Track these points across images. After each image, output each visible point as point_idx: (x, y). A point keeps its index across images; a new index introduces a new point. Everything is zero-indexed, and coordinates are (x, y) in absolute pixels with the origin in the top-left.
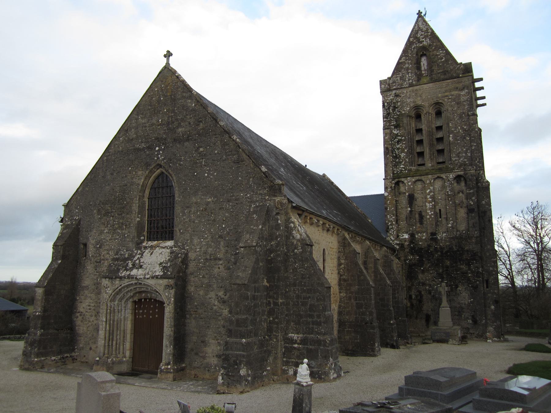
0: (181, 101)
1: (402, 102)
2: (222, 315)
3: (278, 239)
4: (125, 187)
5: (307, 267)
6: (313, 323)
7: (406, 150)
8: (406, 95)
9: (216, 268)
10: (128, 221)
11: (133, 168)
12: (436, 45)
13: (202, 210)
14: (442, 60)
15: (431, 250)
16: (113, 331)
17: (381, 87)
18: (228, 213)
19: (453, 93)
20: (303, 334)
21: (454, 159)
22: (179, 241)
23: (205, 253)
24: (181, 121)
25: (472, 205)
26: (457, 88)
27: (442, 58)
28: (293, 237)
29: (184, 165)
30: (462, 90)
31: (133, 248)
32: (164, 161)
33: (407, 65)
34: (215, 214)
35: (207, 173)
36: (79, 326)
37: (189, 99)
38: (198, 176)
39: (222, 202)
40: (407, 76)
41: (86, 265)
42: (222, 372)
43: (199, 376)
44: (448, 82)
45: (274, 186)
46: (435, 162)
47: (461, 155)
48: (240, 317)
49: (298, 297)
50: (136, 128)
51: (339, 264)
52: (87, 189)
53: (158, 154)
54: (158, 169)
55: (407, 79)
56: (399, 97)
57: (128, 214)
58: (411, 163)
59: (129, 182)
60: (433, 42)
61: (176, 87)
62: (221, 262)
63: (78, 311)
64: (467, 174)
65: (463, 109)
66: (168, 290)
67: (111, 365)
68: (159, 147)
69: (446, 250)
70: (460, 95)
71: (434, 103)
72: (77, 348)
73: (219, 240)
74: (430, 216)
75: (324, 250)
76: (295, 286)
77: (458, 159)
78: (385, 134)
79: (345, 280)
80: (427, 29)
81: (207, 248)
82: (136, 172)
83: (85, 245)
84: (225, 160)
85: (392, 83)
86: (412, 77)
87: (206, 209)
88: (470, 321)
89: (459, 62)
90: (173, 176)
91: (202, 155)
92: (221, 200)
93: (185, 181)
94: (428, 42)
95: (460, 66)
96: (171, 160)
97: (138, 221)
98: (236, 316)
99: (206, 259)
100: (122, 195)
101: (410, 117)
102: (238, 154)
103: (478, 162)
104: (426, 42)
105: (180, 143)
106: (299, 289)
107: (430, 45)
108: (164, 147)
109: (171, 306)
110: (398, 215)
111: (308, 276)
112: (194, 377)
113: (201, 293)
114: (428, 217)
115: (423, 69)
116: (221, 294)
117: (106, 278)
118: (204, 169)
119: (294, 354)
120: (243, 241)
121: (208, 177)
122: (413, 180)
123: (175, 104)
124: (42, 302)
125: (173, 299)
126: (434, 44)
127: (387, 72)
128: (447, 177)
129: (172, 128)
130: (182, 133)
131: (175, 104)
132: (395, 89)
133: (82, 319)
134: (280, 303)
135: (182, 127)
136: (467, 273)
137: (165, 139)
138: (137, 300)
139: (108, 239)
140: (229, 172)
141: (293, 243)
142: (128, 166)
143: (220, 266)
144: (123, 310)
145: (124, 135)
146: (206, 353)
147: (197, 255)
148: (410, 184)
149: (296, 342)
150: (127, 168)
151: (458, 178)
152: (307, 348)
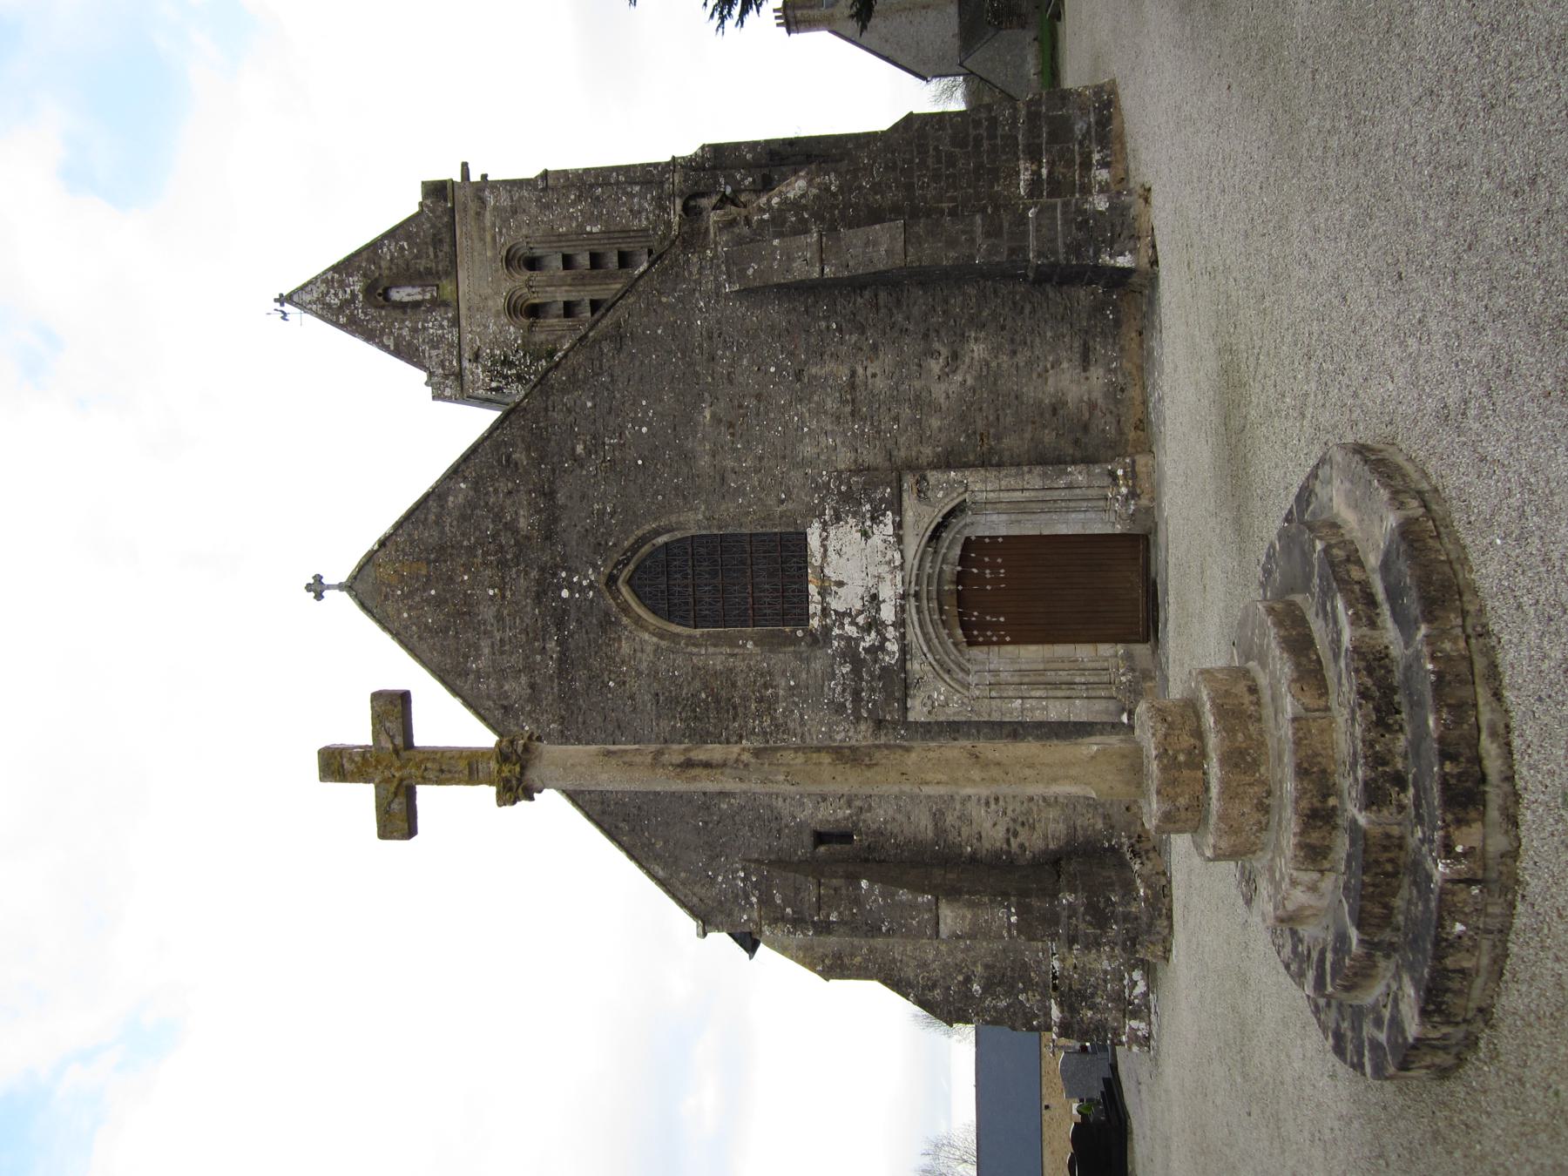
0: (447, 529)
1: (495, 343)
2: (985, 360)
3: (806, 216)
4: (661, 698)
5: (869, 157)
6: (992, 137)
8: (479, 334)
9: (873, 386)
10: (755, 682)
11: (610, 671)
13: (733, 435)
14: (406, 247)
18: (741, 358)
19: (488, 224)
20: (1018, 159)
21: (645, 223)
22: (809, 503)
23: (838, 418)
24: (501, 522)
25: (754, 180)
26: (478, 214)
27: (402, 248)
28: (803, 196)
29: (615, 501)
30: (483, 203)
31: (827, 654)
32: (601, 566)
33: (405, 332)
34: (744, 396)
35: (641, 427)
37: (447, 502)
38: (647, 453)
39: (713, 379)
40: (431, 331)
41: (874, 827)
42: (1108, 258)
43: (1138, 416)
44: (461, 235)
45: (683, 237)
48: (979, 230)
49: (936, 177)
50: (502, 674)
52: (659, 845)
53: (582, 590)
54: (618, 590)
56: (480, 352)
57: (734, 685)
59: (649, 686)
61: (407, 549)
62: (860, 371)
63: (1005, 846)
64: (681, 190)
66: (929, 494)
67: (1137, 674)
68: (561, 589)
70: (495, 208)
71: (507, 268)
72: (1109, 841)
73: (806, 380)
76: (912, 185)
77: (644, 214)
80: (326, 281)
81: (825, 413)
82: (623, 662)
84: (612, 376)
85: (443, 369)
86: (436, 320)
87: (731, 425)
89: (415, 209)
90: (639, 533)
91: (595, 446)
92: (710, 379)
93: (657, 493)
94: (356, 279)
95: (427, 206)
96: (600, 544)
97: (755, 644)
98: (979, 241)
99: (853, 414)
100: (683, 708)
101: (532, 325)
102: (600, 342)
104: (356, 284)
105: (556, 520)
106: (919, 177)
107: (365, 275)
108: (564, 569)
109: (970, 479)
111: (889, 155)
112: (1143, 430)
113: (935, 423)
115: (419, 297)
116: (935, 366)
117: (906, 709)
118: (629, 436)
119: (1063, 174)
120: (808, 271)
121: (649, 425)
123: (453, 547)
124: (979, 905)
125: (953, 473)
129: (515, 549)
130: (532, 515)
131: (453, 547)
132: (460, 361)
133: (1027, 827)
134: (951, 205)
135: (515, 520)
137: (542, 570)
140: (642, 362)
141: (817, 197)
142: (605, 690)
143: (869, 373)
145: (518, 719)
146: (1081, 400)
147: (843, 443)
149: (1037, 173)
150: (610, 696)
152: (1047, 143)
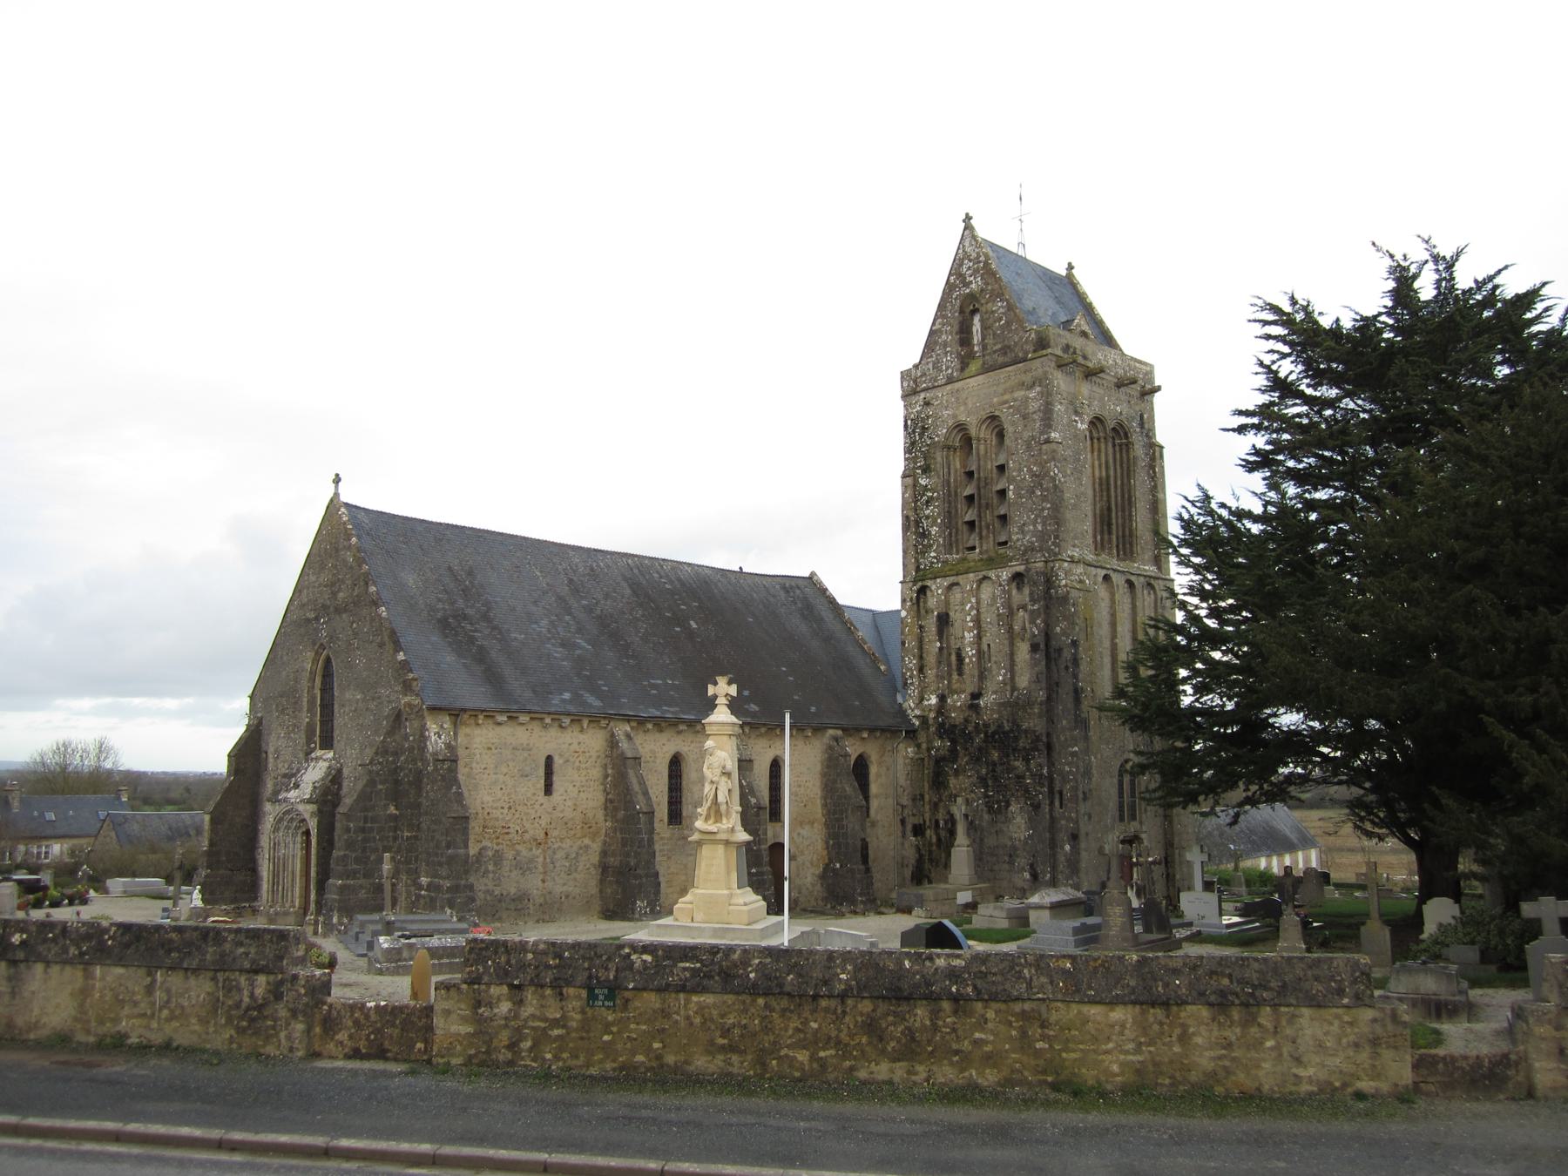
1: (936, 418)
8: (942, 402)
12: (992, 290)
15: (970, 728)
16: (278, 872)
17: (902, 387)
27: (1001, 319)
46: (992, 543)
47: (1026, 529)
51: (606, 776)
58: (949, 546)
60: (987, 284)
65: (1033, 430)
69: (993, 728)
70: (1028, 398)
74: (970, 658)
75: (549, 761)
78: (905, 487)
83: (266, 753)
88: (1027, 875)
103: (1053, 543)
104: (976, 284)
110: (924, 655)
114: (967, 660)
126: (989, 288)
127: (911, 353)
136: (1023, 777)
144: (291, 845)
148: (940, 591)
151: (1018, 578)
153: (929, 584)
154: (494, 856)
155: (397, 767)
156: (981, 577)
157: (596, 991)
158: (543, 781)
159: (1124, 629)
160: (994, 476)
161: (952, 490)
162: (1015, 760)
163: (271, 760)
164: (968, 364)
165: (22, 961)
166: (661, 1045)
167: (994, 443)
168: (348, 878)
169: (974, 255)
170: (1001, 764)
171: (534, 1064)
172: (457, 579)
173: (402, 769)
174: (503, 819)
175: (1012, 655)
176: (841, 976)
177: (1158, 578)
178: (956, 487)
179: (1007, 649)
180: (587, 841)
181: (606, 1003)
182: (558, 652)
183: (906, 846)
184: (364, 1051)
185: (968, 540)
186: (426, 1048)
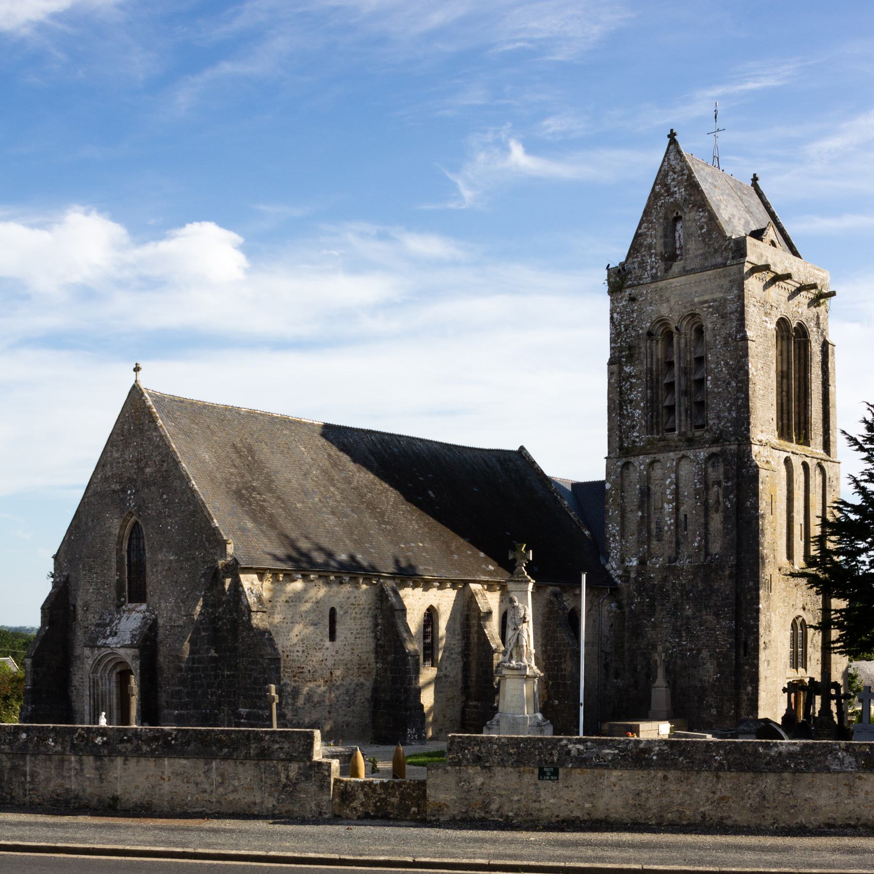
7: (642, 404)
8: (646, 299)
14: (703, 231)
16: (98, 706)
36: (74, 702)
40: (649, 261)
51: (376, 625)
55: (649, 268)
58: (651, 427)
70: (726, 300)
78: (611, 374)
79: (382, 646)
83: (74, 606)
86: (656, 263)
94: (683, 194)
95: (729, 244)
97: (117, 580)
114: (666, 528)
117: (87, 647)
122: (647, 461)
126: (692, 198)
128: (695, 456)
132: (630, 286)
138: (786, 687)
139: (93, 600)
148: (642, 467)
153: (632, 460)
154: (292, 691)
155: (215, 617)
156: (680, 456)
157: (545, 769)
158: (328, 630)
159: (816, 510)
160: (693, 366)
161: (654, 377)
162: (706, 615)
163: (80, 611)
164: (671, 267)
165: (105, 756)
166: (591, 805)
167: (693, 338)
168: (181, 709)
169: (678, 168)
170: (694, 618)
171: (500, 820)
172: (241, 455)
173: (220, 619)
174: (299, 661)
175: (706, 525)
176: (716, 758)
177: (827, 461)
178: (658, 375)
179: (702, 520)
180: (362, 680)
181: (552, 778)
182: (332, 521)
183: (609, 687)
184: (372, 814)
185: (667, 423)
186: (418, 810)
